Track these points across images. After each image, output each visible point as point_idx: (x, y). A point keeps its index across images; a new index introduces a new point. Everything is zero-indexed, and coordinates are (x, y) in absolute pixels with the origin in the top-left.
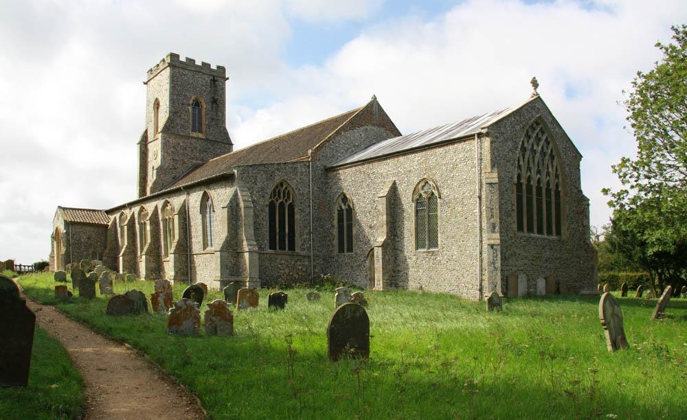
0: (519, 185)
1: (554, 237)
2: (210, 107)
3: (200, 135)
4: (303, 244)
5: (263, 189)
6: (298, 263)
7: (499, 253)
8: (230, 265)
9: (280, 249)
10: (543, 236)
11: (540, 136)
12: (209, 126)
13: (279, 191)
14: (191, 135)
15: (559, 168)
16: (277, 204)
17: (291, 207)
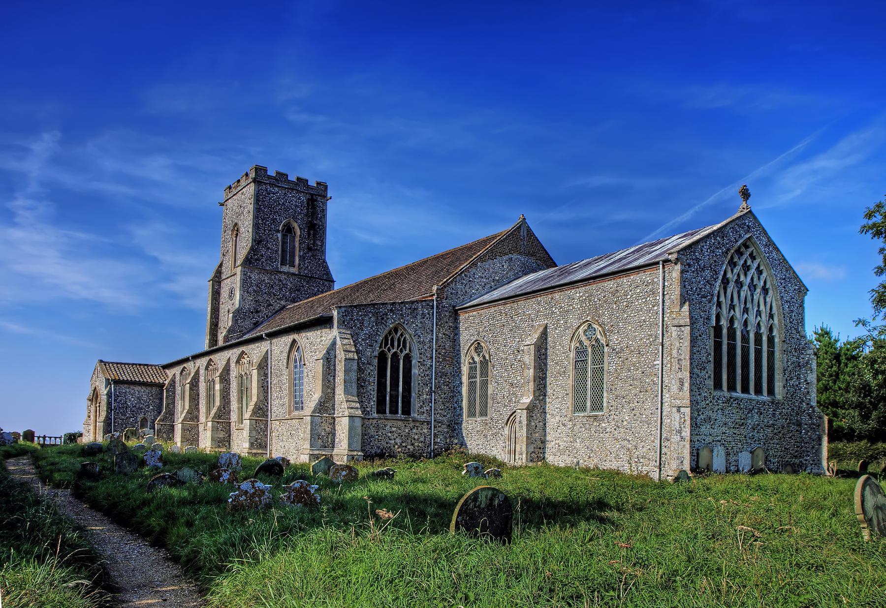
3: (292, 270)
4: (421, 407)
5: (370, 336)
6: (414, 431)
16: (390, 356)
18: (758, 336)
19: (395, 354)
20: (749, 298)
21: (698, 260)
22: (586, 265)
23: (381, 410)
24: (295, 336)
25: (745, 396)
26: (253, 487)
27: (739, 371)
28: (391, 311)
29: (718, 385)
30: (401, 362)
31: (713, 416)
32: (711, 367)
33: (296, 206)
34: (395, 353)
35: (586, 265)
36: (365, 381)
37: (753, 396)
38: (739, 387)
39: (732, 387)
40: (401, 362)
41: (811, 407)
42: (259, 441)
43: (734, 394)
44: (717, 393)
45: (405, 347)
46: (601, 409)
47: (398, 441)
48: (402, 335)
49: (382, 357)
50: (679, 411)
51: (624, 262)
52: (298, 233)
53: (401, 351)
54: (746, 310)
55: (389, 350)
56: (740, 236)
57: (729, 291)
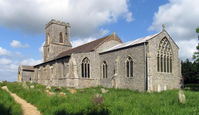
3: (62, 44)
4: (92, 76)
18: (168, 59)
19: (86, 64)
20: (162, 50)
21: (153, 42)
22: (129, 43)
23: (83, 76)
24: (84, 55)
25: (165, 73)
26: (30, 87)
27: (163, 67)
28: (84, 54)
29: (158, 70)
30: (87, 66)
31: (158, 78)
32: (157, 67)
35: (129, 43)
36: (79, 70)
37: (167, 73)
38: (163, 71)
39: (162, 71)
40: (87, 66)
43: (162, 73)
44: (158, 72)
45: (88, 62)
46: (133, 76)
47: (87, 84)
49: (82, 64)
51: (137, 42)
54: (165, 53)
56: (163, 36)
57: (161, 49)
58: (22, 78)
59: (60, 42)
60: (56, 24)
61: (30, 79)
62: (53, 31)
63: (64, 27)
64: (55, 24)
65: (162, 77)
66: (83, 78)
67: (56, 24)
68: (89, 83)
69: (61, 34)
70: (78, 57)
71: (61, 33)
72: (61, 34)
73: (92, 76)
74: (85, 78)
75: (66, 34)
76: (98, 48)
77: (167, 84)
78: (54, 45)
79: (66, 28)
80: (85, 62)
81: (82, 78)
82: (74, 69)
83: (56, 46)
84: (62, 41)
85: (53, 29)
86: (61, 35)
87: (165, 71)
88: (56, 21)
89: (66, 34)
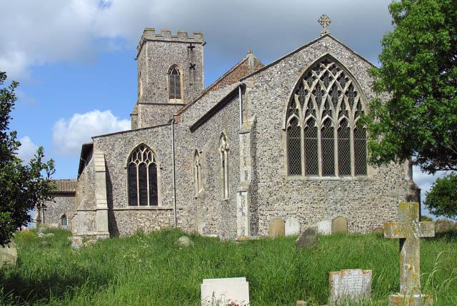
0: (292, 130)
1: (352, 177)
2: (188, 73)
3: (179, 101)
4: (165, 199)
5: (120, 154)
6: (160, 216)
7: (246, 199)
8: (88, 221)
9: (140, 205)
10: (349, 178)
11: (331, 74)
12: (187, 92)
13: (140, 154)
14: (170, 102)
15: (362, 103)
16: (138, 166)
17: (153, 166)
33: (179, 53)
34: (143, 163)
41: (406, 181)
42: (254, 224)
43: (313, 178)
48: (147, 151)
50: (241, 194)
52: (182, 73)
53: (147, 162)
55: (137, 162)
58: (39, 216)
59: (171, 97)
60: (158, 41)
61: (64, 216)
62: (147, 64)
63: (185, 47)
64: (152, 43)
65: (313, 193)
66: (133, 207)
67: (158, 41)
68: (154, 221)
69: (174, 71)
70: (113, 146)
71: (174, 66)
72: (174, 71)
73: (165, 199)
74: (148, 207)
75: (192, 67)
76: (188, 111)
77: (335, 216)
78: (150, 109)
79: (192, 48)
80: (140, 159)
81: (129, 207)
82: (98, 184)
83: (158, 109)
84: (179, 92)
85: (147, 59)
86: (175, 72)
87: (328, 171)
88: (157, 32)
89: (192, 67)
